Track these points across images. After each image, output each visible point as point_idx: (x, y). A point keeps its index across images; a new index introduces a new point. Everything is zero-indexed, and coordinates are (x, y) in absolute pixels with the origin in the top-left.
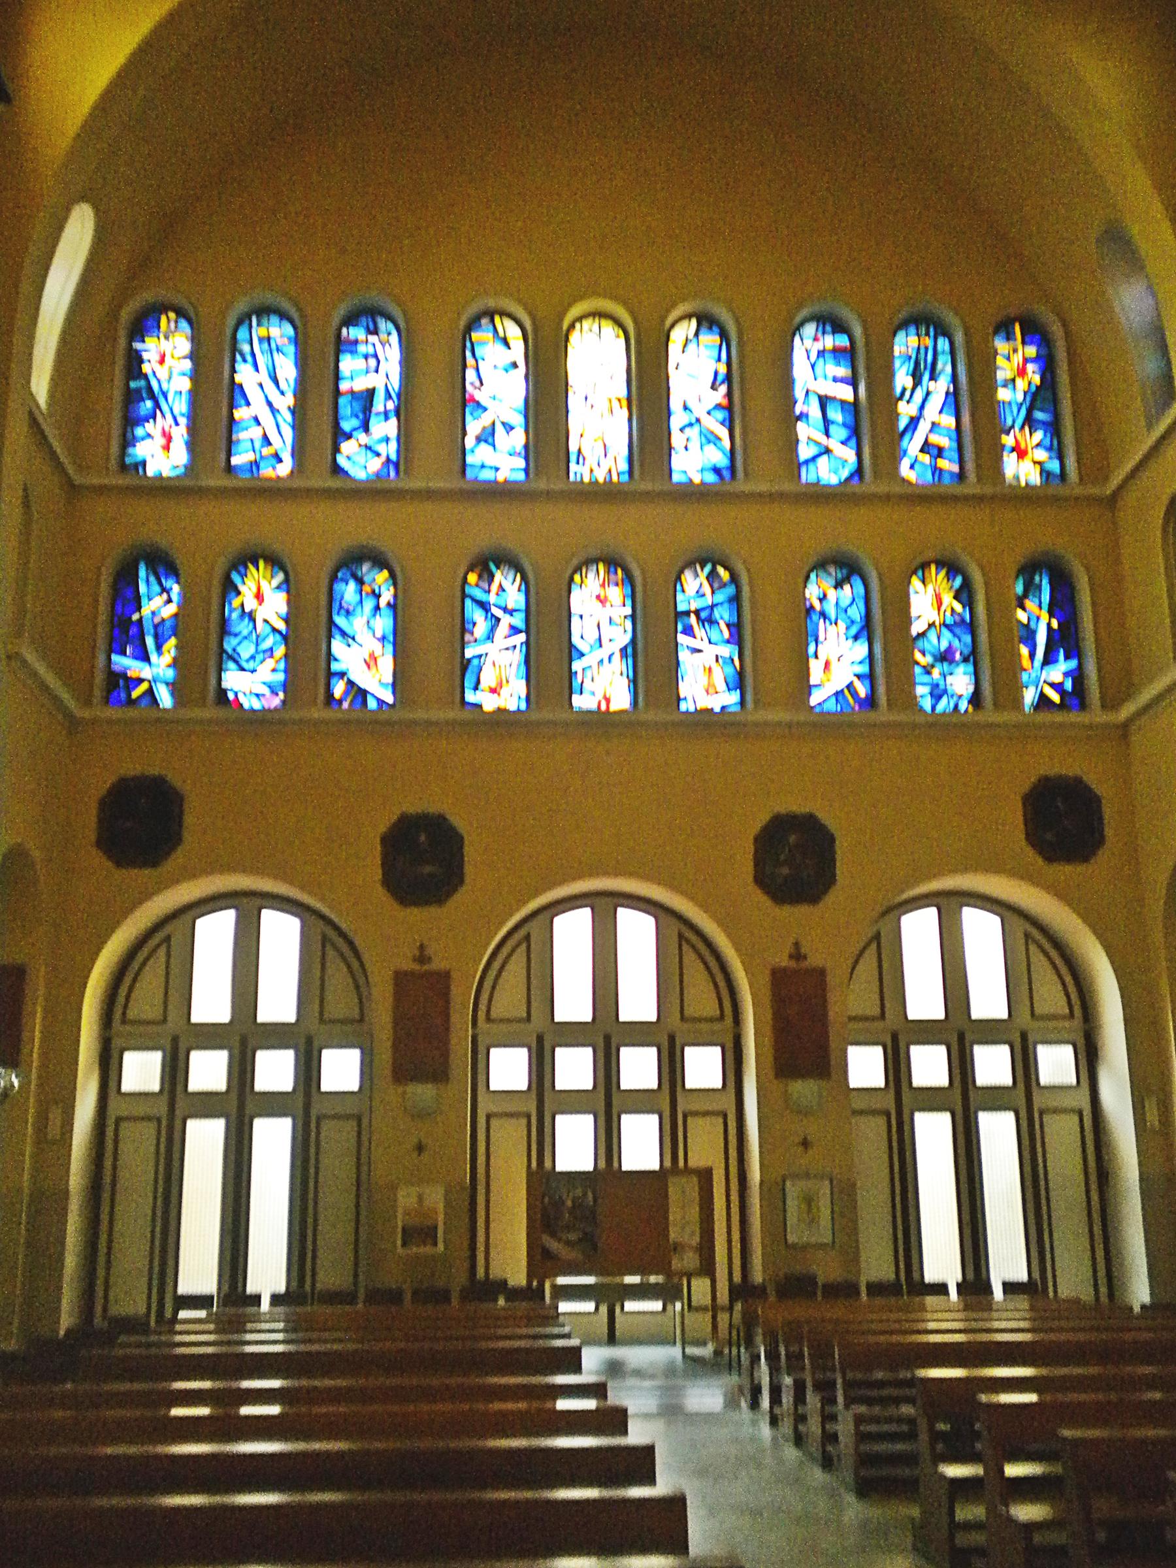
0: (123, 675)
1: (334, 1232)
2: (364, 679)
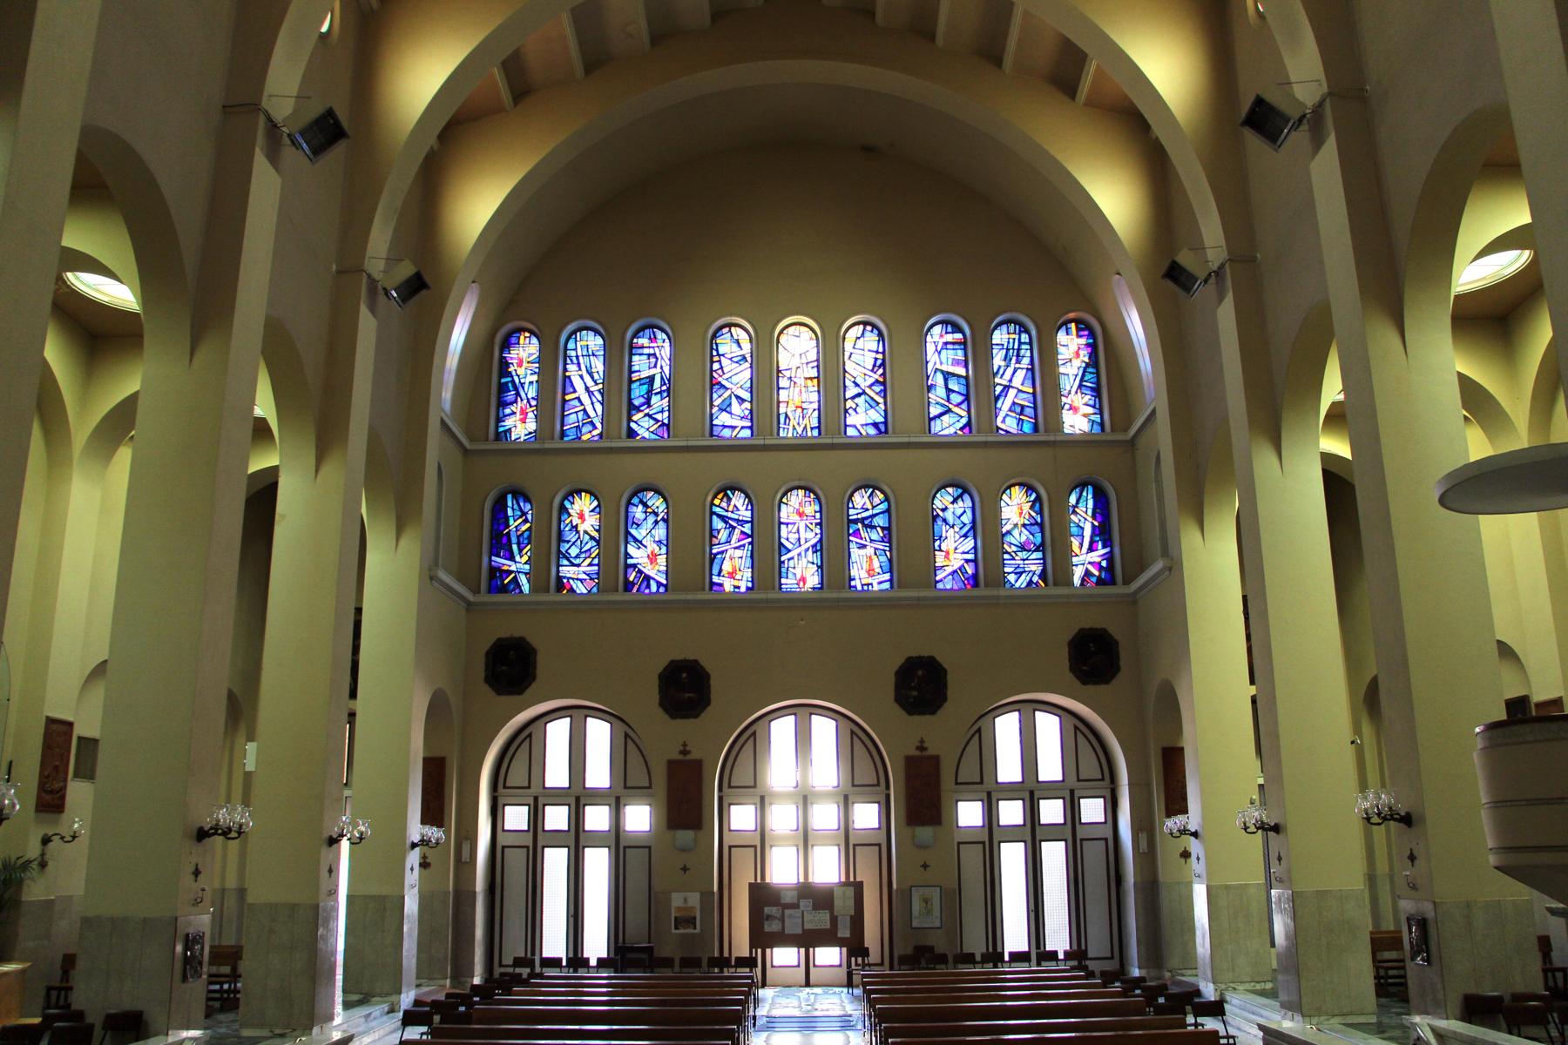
0: (499, 569)
1: (636, 917)
2: (649, 570)
